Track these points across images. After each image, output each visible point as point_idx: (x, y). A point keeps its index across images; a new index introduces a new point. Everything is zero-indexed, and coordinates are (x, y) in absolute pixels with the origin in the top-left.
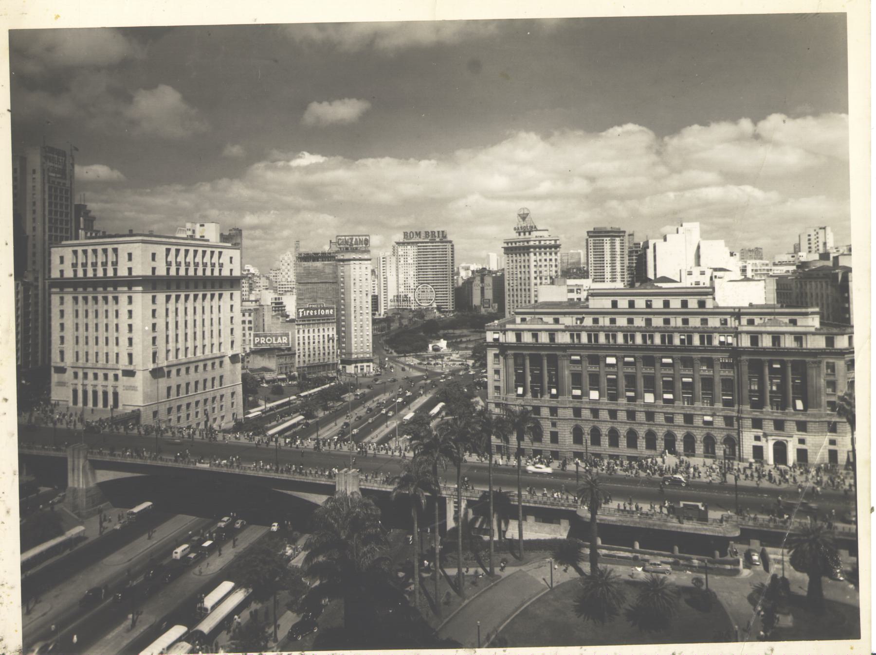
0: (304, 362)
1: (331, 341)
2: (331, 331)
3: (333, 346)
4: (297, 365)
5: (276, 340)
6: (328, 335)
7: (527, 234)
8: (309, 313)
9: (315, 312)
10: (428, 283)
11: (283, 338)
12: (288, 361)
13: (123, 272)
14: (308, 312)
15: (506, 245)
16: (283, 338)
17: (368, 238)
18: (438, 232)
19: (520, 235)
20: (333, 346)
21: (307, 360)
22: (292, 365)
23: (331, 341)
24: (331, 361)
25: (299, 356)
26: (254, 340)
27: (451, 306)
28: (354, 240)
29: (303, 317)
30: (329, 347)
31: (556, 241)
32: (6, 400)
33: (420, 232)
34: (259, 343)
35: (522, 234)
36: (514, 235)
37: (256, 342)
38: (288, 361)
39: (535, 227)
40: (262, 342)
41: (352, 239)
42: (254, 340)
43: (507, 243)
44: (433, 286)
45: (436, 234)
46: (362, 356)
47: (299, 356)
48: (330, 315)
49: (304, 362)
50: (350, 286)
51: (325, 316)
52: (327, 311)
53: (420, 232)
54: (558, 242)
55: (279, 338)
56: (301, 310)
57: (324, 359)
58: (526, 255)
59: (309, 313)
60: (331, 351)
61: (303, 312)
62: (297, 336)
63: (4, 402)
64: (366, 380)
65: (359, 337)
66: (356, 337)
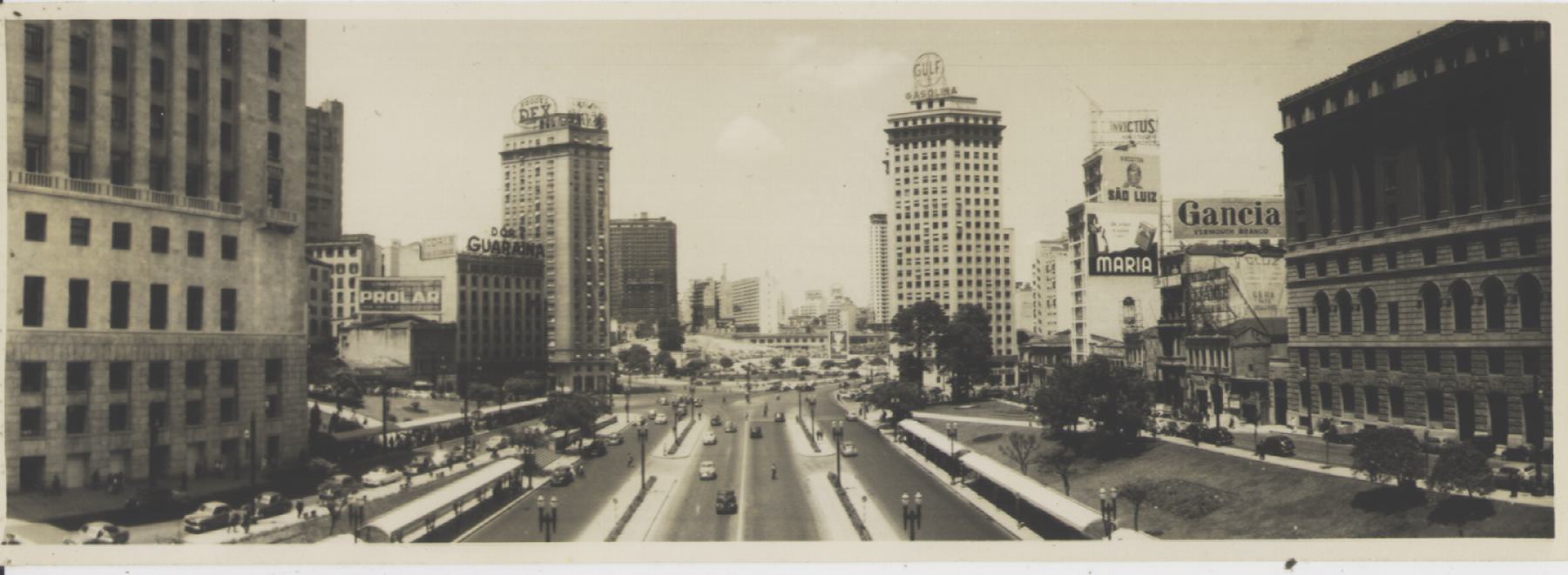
7: (936, 105)
15: (892, 126)
19: (919, 105)
35: (925, 107)
36: (908, 109)
39: (954, 91)
43: (896, 123)
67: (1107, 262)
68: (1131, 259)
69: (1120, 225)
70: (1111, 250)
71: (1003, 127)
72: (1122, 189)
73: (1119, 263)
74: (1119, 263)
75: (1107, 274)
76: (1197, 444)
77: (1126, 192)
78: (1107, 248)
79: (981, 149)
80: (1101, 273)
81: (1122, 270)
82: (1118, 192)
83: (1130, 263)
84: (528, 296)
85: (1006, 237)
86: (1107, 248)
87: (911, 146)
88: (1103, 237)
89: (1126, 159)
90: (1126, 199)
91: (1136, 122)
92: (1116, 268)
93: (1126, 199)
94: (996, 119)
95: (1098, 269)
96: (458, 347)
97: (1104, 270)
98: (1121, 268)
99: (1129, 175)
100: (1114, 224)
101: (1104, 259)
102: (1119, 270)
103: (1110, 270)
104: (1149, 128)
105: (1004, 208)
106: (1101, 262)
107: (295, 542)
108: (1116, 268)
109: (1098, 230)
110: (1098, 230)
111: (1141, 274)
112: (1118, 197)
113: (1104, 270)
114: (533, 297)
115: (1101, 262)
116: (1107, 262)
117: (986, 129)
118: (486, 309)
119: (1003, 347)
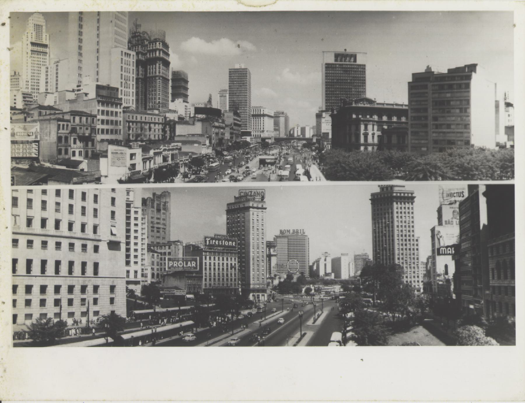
0: (210, 284)
1: (233, 269)
2: (234, 261)
3: (235, 274)
4: (203, 287)
5: (187, 264)
6: (231, 264)
8: (215, 243)
9: (221, 244)
10: (295, 259)
11: (193, 262)
12: (195, 282)
13: (262, 113)
14: (214, 241)
16: (193, 262)
17: (263, 191)
18: (301, 230)
20: (234, 273)
21: (212, 283)
22: (200, 287)
23: (233, 269)
24: (233, 287)
25: (206, 280)
26: (168, 264)
27: (308, 274)
28: (253, 193)
29: (210, 245)
30: (231, 274)
31: (412, 194)
32: (4, 303)
33: (290, 230)
34: (172, 266)
37: (170, 265)
38: (195, 282)
40: (175, 265)
41: (251, 192)
42: (168, 264)
44: (297, 260)
45: (299, 231)
46: (258, 286)
47: (206, 280)
48: (232, 247)
49: (210, 284)
50: (249, 228)
51: (229, 246)
52: (230, 243)
53: (290, 230)
54: (414, 195)
55: (189, 263)
56: (208, 239)
57: (227, 284)
58: (403, 203)
59: (215, 243)
60: (233, 278)
61: (209, 241)
62: (204, 261)
63: (3, 305)
64: (288, 234)
65: (256, 252)
66: (253, 234)
67: (444, 250)
68: (176, 262)
69: (450, 235)
70: (446, 245)
71: (415, 197)
72: (450, 220)
73: (449, 250)
74: (449, 250)
75: (445, 254)
76: (123, 331)
77: (452, 221)
78: (444, 244)
79: (407, 205)
80: (442, 254)
81: (451, 253)
82: (449, 221)
83: (175, 263)
84: (231, 264)
85: (417, 240)
86: (444, 244)
87: (403, 203)
88: (443, 240)
89: (452, 208)
90: (452, 224)
91: (457, 193)
92: (448, 252)
93: (452, 224)
94: (412, 194)
95: (441, 253)
96: (204, 282)
97: (443, 253)
98: (450, 252)
99: (453, 214)
100: (447, 234)
101: (443, 249)
102: (449, 253)
103: (446, 253)
104: (462, 195)
105: (416, 229)
106: (442, 250)
107: (216, 346)
108: (448, 252)
109: (441, 237)
110: (441, 237)
111: (447, 254)
112: (449, 223)
113: (443, 253)
114: (233, 265)
115: (442, 250)
116: (444, 250)
117: (408, 198)
118: (223, 269)
119: (416, 284)
